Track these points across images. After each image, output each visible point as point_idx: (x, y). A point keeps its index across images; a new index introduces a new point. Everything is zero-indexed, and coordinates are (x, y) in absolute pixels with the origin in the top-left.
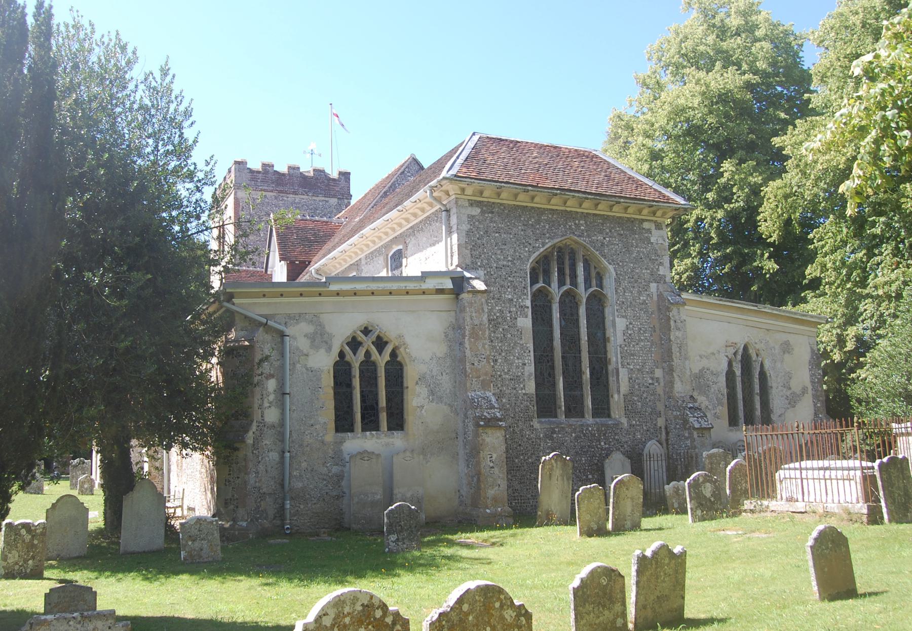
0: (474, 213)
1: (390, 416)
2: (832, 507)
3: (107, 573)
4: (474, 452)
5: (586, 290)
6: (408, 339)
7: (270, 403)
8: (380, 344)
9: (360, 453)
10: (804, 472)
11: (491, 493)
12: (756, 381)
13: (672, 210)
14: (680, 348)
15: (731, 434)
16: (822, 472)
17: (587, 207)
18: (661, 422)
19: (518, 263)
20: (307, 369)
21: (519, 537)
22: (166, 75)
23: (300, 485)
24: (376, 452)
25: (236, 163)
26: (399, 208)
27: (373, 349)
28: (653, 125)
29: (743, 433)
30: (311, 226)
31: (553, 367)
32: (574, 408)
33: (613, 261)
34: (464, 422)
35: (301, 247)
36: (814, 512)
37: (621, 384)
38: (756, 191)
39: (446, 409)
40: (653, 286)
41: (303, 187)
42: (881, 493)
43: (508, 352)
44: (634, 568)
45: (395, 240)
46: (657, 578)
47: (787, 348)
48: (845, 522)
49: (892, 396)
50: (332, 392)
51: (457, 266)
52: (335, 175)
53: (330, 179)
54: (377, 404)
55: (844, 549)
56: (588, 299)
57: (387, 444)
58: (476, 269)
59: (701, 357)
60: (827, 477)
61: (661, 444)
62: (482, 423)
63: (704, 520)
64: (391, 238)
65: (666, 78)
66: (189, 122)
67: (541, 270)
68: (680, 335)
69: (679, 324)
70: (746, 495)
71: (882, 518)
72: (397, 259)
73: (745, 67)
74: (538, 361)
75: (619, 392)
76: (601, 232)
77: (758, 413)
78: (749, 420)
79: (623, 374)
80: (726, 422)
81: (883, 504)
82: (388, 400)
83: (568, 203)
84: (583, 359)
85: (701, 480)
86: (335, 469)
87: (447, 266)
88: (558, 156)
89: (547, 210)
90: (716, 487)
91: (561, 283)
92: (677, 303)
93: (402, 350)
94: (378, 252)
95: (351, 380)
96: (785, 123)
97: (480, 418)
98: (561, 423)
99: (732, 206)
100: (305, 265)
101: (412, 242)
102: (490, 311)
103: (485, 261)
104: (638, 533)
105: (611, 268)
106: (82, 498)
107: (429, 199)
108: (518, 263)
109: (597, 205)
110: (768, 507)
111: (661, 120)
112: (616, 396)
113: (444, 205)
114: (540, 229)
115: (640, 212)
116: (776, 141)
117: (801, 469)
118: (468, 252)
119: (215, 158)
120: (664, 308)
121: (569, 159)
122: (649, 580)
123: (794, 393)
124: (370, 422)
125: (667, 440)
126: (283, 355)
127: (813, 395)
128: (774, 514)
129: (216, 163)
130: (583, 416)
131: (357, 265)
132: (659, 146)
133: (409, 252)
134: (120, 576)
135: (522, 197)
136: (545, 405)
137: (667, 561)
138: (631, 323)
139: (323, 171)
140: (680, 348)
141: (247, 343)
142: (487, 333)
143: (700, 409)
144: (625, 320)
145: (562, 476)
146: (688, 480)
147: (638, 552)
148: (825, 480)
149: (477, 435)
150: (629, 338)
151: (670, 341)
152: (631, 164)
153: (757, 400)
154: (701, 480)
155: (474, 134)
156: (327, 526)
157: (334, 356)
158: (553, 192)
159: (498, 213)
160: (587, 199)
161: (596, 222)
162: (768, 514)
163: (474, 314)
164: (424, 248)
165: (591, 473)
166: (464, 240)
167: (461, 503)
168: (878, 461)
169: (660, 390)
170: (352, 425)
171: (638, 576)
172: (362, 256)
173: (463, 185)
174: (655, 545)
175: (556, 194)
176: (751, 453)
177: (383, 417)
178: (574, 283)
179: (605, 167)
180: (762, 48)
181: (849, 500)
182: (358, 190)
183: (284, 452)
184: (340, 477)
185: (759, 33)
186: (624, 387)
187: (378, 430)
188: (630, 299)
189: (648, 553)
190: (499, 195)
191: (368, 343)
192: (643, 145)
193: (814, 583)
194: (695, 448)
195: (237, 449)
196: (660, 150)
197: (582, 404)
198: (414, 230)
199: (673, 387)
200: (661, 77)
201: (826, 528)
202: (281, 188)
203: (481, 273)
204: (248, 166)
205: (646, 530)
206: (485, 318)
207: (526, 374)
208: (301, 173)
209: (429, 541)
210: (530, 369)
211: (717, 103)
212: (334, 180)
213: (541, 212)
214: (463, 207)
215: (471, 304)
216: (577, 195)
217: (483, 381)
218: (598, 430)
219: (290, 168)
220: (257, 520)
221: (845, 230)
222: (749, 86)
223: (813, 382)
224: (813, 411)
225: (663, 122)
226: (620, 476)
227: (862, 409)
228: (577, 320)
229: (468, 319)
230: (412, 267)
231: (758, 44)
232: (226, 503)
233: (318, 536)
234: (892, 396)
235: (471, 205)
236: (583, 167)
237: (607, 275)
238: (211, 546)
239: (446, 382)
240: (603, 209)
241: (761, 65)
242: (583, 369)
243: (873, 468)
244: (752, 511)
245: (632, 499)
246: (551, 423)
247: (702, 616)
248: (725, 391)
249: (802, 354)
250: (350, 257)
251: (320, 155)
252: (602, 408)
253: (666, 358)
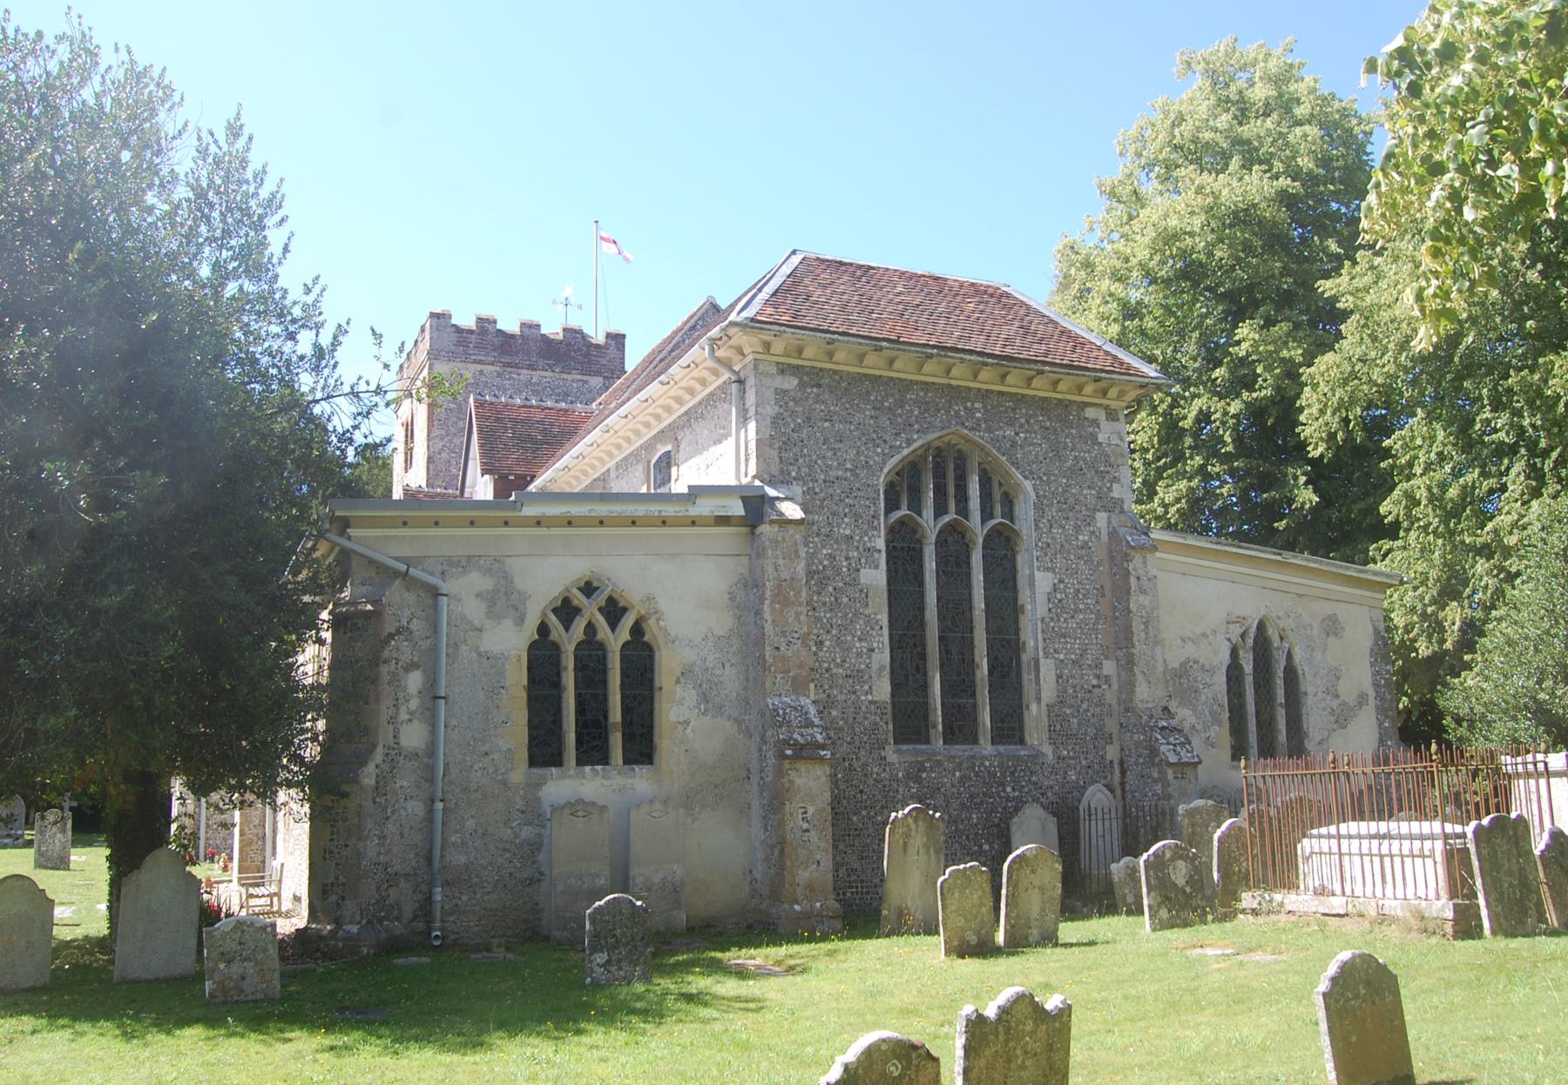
0: (786, 386)
1: (628, 738)
2: (1393, 906)
3: (61, 1022)
4: (776, 802)
5: (983, 522)
6: (663, 604)
7: (412, 713)
8: (614, 611)
9: (569, 804)
10: (1344, 842)
11: (804, 875)
12: (1279, 682)
13: (1135, 388)
14: (1146, 624)
16: (1375, 843)
17: (987, 379)
18: (1112, 753)
19: (863, 473)
20: (479, 654)
21: (841, 957)
22: (237, 136)
23: (463, 859)
24: (600, 802)
25: (433, 315)
26: (662, 378)
27: (601, 622)
28: (1127, 260)
29: (1243, 774)
30: (539, 416)
31: (923, 656)
32: (960, 728)
33: (1031, 472)
34: (760, 749)
35: (518, 447)
36: (1362, 916)
37: (1044, 684)
38: (1291, 373)
39: (729, 727)
40: (1101, 518)
41: (544, 357)
42: (1479, 882)
43: (844, 628)
44: (960, 1041)
45: (661, 436)
46: (1009, 1061)
47: (1332, 626)
48: (1414, 934)
49: (1512, 711)
50: (524, 695)
51: (754, 477)
52: (600, 339)
53: (591, 345)
54: (606, 717)
55: (1390, 998)
56: (987, 538)
57: (622, 789)
58: (789, 483)
60: (1406, 851)
61: (1112, 791)
62: (789, 752)
63: (1172, 927)
64: (655, 432)
65: (1150, 187)
66: (277, 218)
67: (904, 486)
69: (1145, 583)
70: (1246, 881)
71: (1480, 926)
72: (665, 465)
73: (1278, 166)
74: (897, 644)
75: (1039, 700)
76: (1010, 423)
77: (1282, 737)
78: (1267, 750)
79: (1048, 669)
80: (1226, 753)
81: (1481, 901)
82: (626, 709)
83: (954, 372)
84: (976, 642)
85: (1168, 855)
86: (527, 832)
87: (738, 478)
88: (940, 292)
89: (917, 382)
90: (1195, 868)
91: (940, 510)
92: (1142, 547)
93: (652, 622)
94: (635, 455)
95: (559, 674)
96: (1338, 261)
97: (786, 743)
98: (935, 754)
99: (1255, 395)
100: (524, 481)
101: (686, 437)
102: (811, 557)
103: (805, 470)
104: (1049, 951)
105: (1028, 485)
106: (47, 880)
107: (710, 363)
108: (863, 473)
109: (1004, 376)
110: (1281, 904)
111: (1141, 251)
112: (1034, 707)
113: (737, 373)
114: (912, 425)
115: (1080, 389)
116: (1326, 287)
117: (1339, 837)
118: (775, 453)
119: (321, 282)
120: (1119, 555)
121: (959, 299)
122: (990, 1066)
123: (1344, 703)
124: (594, 748)
125: (1123, 784)
126: (435, 629)
127: (1377, 708)
128: (1293, 918)
129: (323, 290)
130: (975, 742)
131: (603, 479)
132: (1134, 295)
133: (681, 456)
134: (84, 1026)
135: (871, 359)
136: (908, 721)
137: (1029, 1026)
138: (1061, 581)
139: (580, 332)
140: (1146, 624)
141: (369, 607)
142: (804, 594)
143: (1180, 731)
144: (1051, 575)
145: (927, 847)
146: (1145, 856)
147: (968, 1009)
148: (1362, 855)
149: (780, 773)
150: (1057, 605)
151: (1129, 611)
152: (1093, 327)
153: (1281, 714)
154: (1168, 855)
155: (794, 252)
156: (510, 933)
157: (530, 632)
158: (927, 352)
159: (829, 386)
160: (986, 364)
161: (1003, 406)
162: (1283, 917)
163: (781, 561)
164: (705, 449)
165: (987, 841)
166: (768, 432)
167: (754, 893)
168: (1473, 824)
169: (1111, 698)
170: (560, 754)
171: (967, 1056)
172: (611, 464)
173: (767, 337)
174: (1005, 995)
175: (931, 356)
176: (1263, 807)
177: (616, 740)
178: (963, 510)
179: (1022, 312)
180: (1305, 135)
181: (1421, 893)
182: (633, 357)
183: (433, 801)
184: (535, 846)
185: (1301, 111)
186: (1048, 692)
187: (607, 763)
188: (1060, 539)
189: (991, 1012)
190: (831, 355)
191: (591, 610)
192: (1111, 295)
193: (1330, 1066)
194: (1170, 797)
195: (345, 795)
196: (1138, 303)
197: (975, 720)
198: (690, 418)
199: (1133, 692)
200: (1141, 184)
201: (1354, 957)
203: (797, 489)
204: (454, 321)
205: (1065, 945)
206: (801, 568)
207: (875, 667)
208: (543, 336)
209: (678, 964)
210: (883, 657)
211: (1231, 226)
212: (598, 346)
213: (908, 385)
214: (767, 374)
215: (775, 543)
216: (968, 357)
217: (794, 679)
218: (1001, 766)
219: (523, 325)
220: (380, 921)
221: (1441, 435)
222: (1284, 198)
223: (1376, 685)
224: (1377, 736)
225: (1143, 254)
226: (1030, 846)
227: (1462, 731)
228: (968, 576)
229: (770, 569)
230: (684, 478)
231: (1298, 130)
232: (324, 892)
233: (489, 950)
234: (1512, 711)
236: (982, 312)
237: (1021, 497)
238: (264, 977)
239: (731, 681)
240: (1014, 383)
241: (1305, 163)
242: (977, 659)
243: (1464, 835)
244: (1254, 912)
245: (1042, 889)
246: (917, 752)
249: (1359, 635)
250: (593, 467)
251: (580, 307)
252: (1009, 727)
253: (1122, 641)
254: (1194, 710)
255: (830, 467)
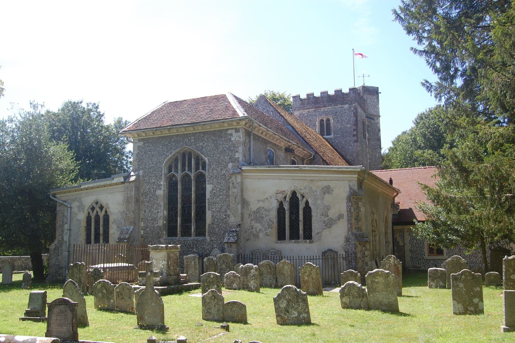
0: (140, 145)
6: (110, 205)
8: (101, 208)
15: (277, 245)
17: (191, 130)
27: (99, 210)
32: (186, 232)
33: (208, 155)
40: (230, 165)
59: (258, 201)
68: (236, 191)
91: (183, 170)
105: (206, 159)
118: (137, 163)
123: (331, 219)
178: (190, 169)
202: (317, 105)
207: (159, 217)
247: (29, 322)
248: (275, 221)
251: (369, 76)
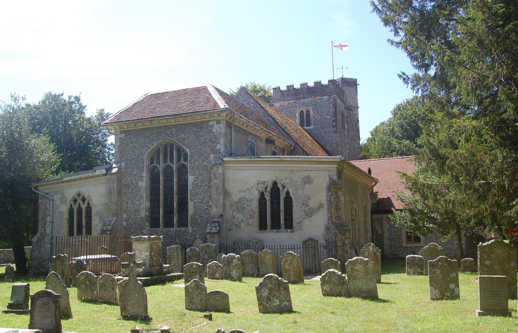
0: (122, 137)
6: (92, 197)
8: (84, 200)
27: (81, 202)
32: (169, 223)
33: (189, 146)
59: (240, 192)
68: (217, 182)
91: (165, 161)
108: (140, 156)
123: (311, 208)
144: (193, 176)
150: (195, 185)
161: (181, 128)
178: (172, 161)
202: (296, 97)
207: (141, 208)
235: (121, 133)
248: (257, 211)
251: (347, 68)
254: (243, 214)
255: (132, 156)
